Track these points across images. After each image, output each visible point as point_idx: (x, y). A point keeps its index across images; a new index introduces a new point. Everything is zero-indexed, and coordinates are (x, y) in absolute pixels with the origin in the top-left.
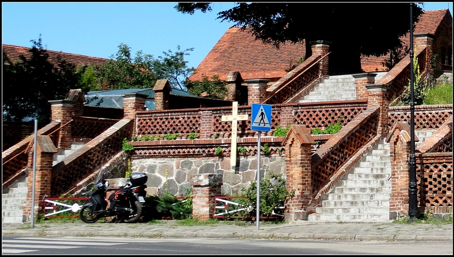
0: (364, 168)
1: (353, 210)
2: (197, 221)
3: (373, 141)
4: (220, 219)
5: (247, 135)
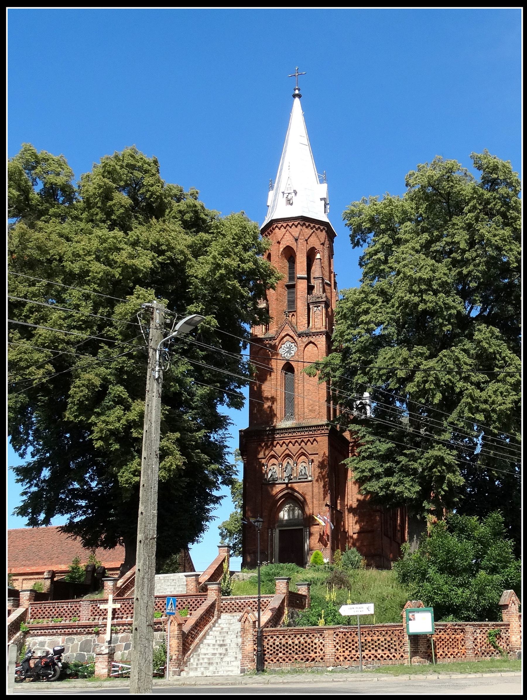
0: (209, 640)
1: (212, 668)
2: (98, 679)
3: (213, 621)
4: (116, 677)
5: (117, 618)
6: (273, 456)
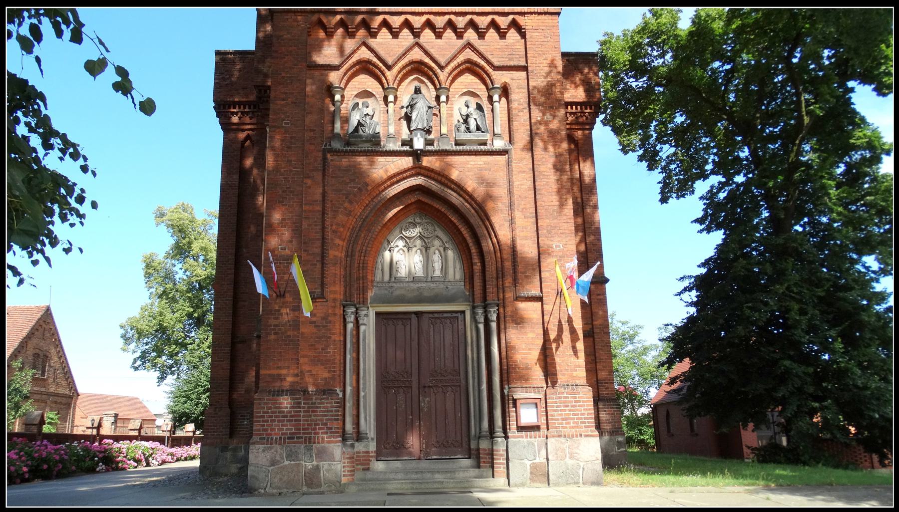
6: (365, 67)
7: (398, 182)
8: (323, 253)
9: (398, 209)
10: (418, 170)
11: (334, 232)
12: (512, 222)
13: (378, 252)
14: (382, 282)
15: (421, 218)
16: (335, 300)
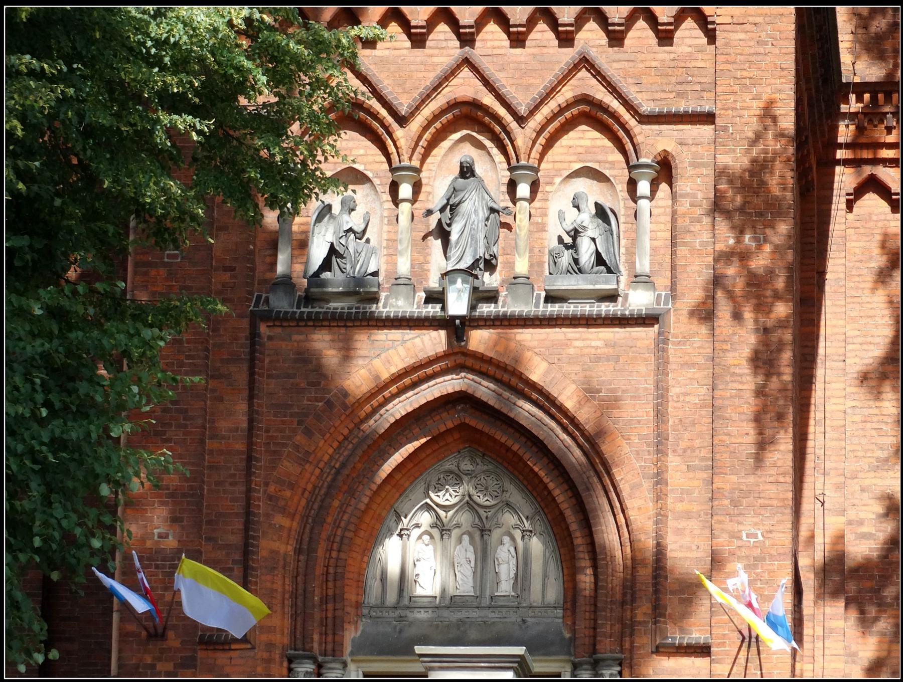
7: (414, 385)
8: (246, 545)
9: (417, 444)
10: (460, 359)
11: (270, 498)
12: (660, 479)
13: (374, 539)
14: (382, 606)
15: (473, 461)
16: (270, 646)
